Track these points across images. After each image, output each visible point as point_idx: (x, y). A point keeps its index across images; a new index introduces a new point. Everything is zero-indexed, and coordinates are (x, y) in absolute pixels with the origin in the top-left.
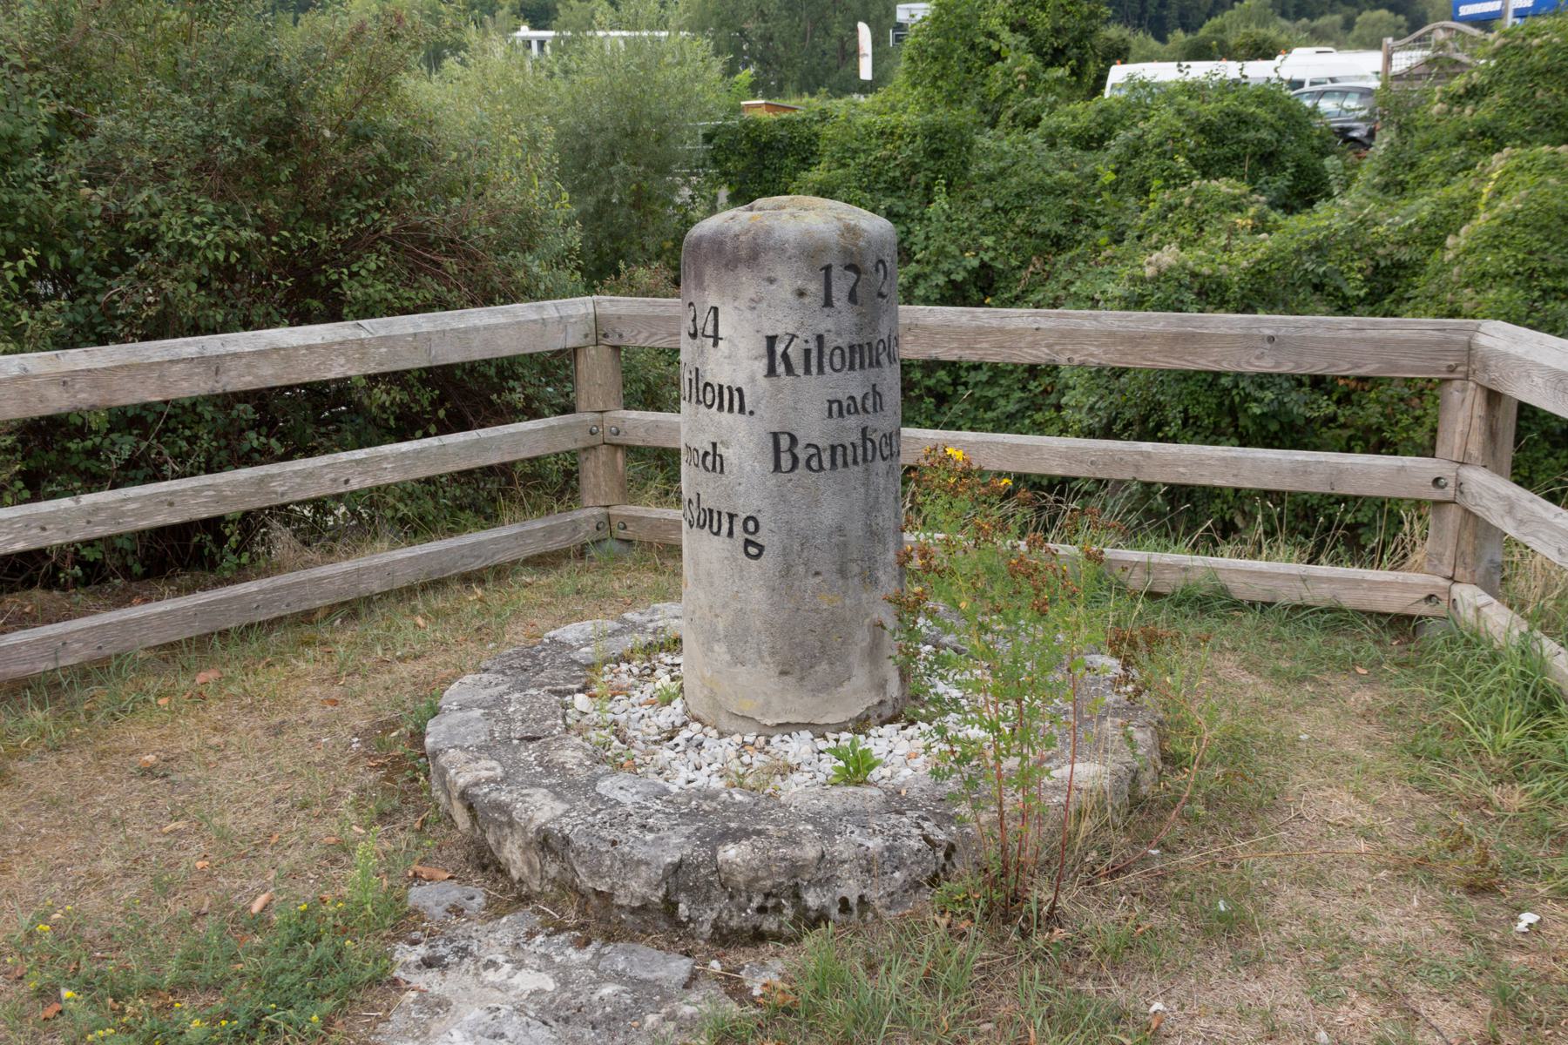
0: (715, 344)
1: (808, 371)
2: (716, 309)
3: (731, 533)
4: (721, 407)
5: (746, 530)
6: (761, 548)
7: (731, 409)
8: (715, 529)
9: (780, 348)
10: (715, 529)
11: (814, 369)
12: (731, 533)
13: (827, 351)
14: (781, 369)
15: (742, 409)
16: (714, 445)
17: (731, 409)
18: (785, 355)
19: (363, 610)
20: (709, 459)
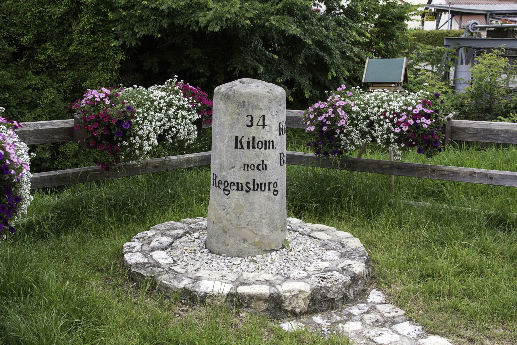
0: (263, 127)
1: (248, 148)
2: (264, 116)
3: (269, 189)
4: (266, 148)
5: (274, 187)
6: (277, 191)
7: (269, 148)
8: (263, 189)
9: (239, 139)
10: (263, 189)
11: (251, 147)
12: (269, 189)
13: (256, 142)
14: (239, 146)
15: (273, 148)
16: (263, 161)
17: (269, 148)
18: (241, 141)
19: (464, 147)
20: (261, 166)
